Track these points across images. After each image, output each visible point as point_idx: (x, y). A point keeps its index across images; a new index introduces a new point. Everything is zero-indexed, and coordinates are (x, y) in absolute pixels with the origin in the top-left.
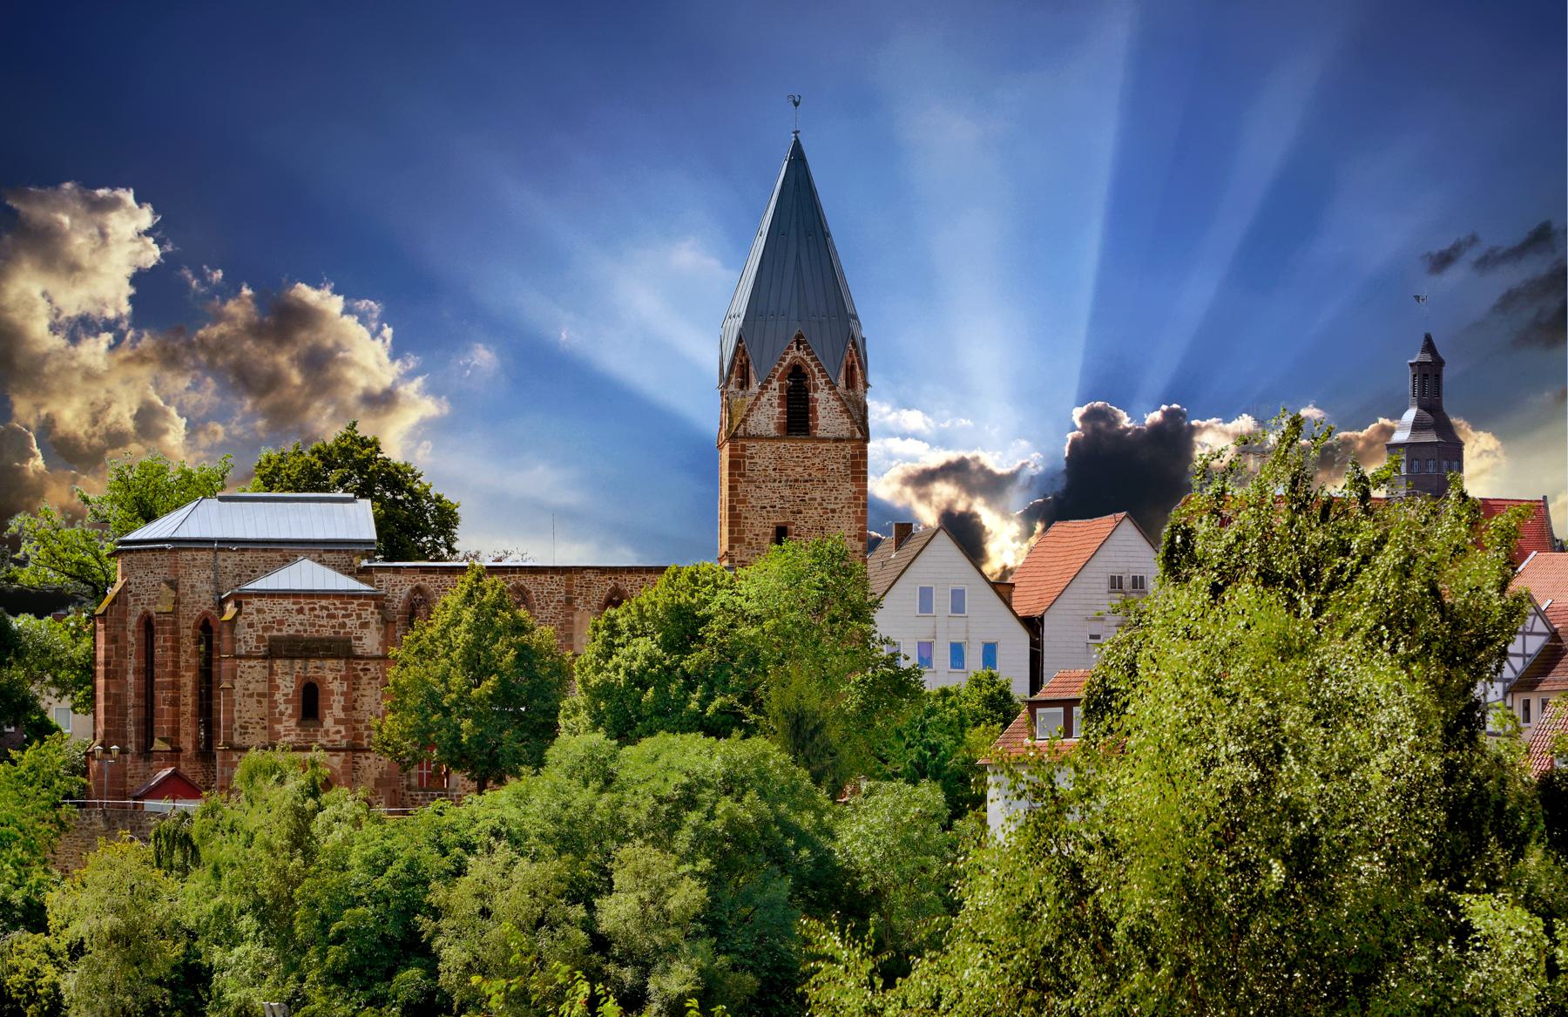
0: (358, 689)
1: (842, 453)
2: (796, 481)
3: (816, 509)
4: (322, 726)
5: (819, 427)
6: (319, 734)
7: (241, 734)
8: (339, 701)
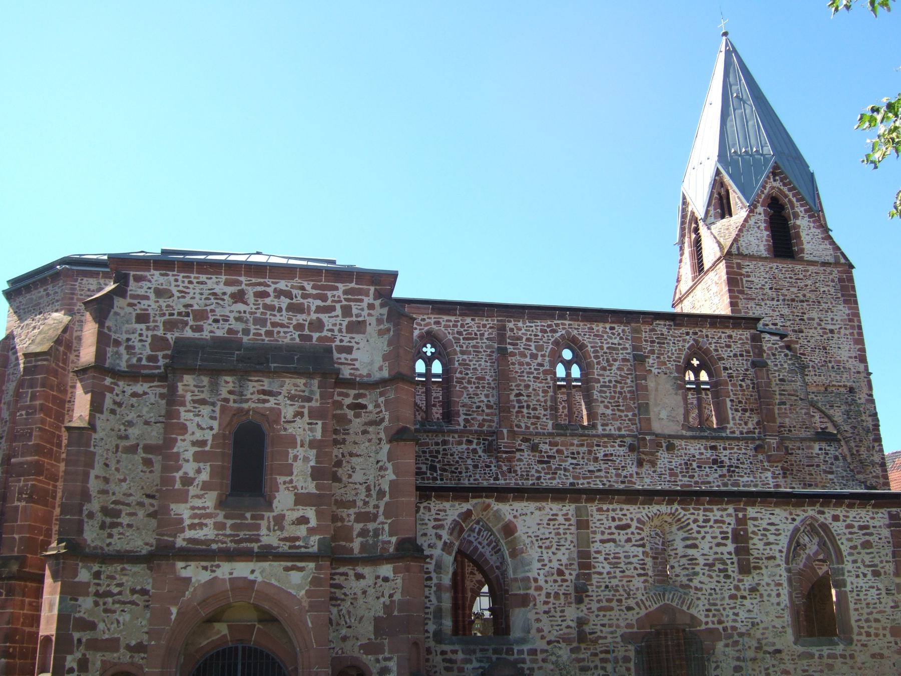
0: (344, 442)
1: (831, 277)
2: (793, 300)
3: (816, 328)
4: (269, 506)
5: (806, 251)
6: (264, 524)
7: (103, 526)
8: (306, 459)
